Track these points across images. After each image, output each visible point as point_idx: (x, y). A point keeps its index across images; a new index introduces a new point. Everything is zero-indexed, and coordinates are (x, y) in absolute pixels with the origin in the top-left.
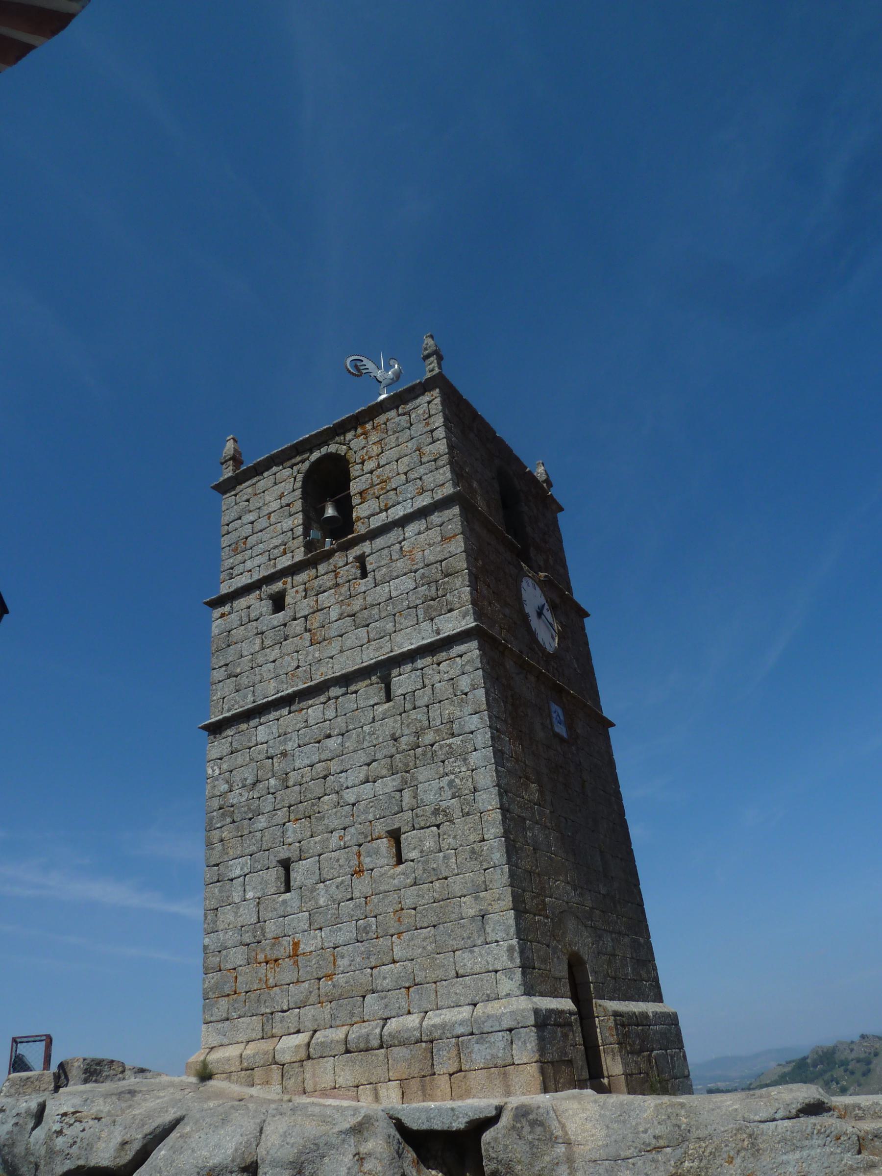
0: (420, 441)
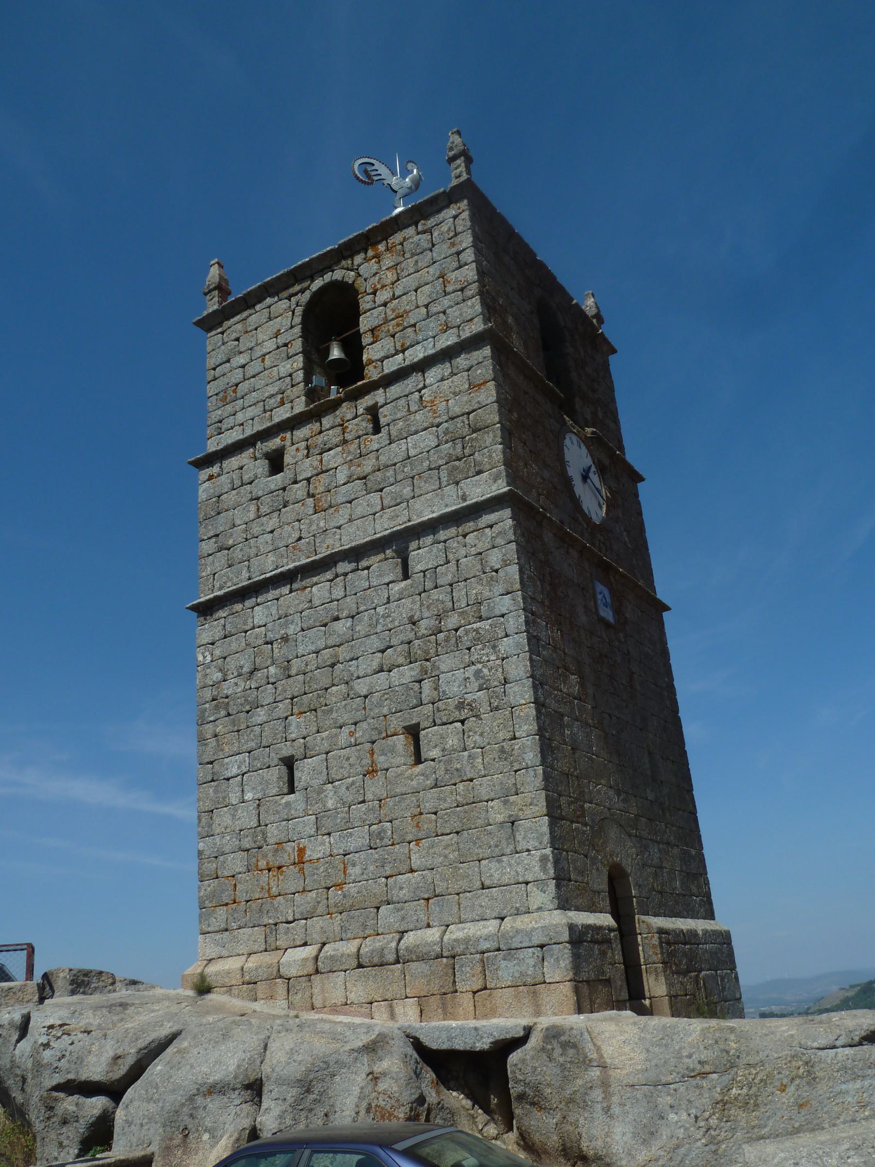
0: (444, 266)
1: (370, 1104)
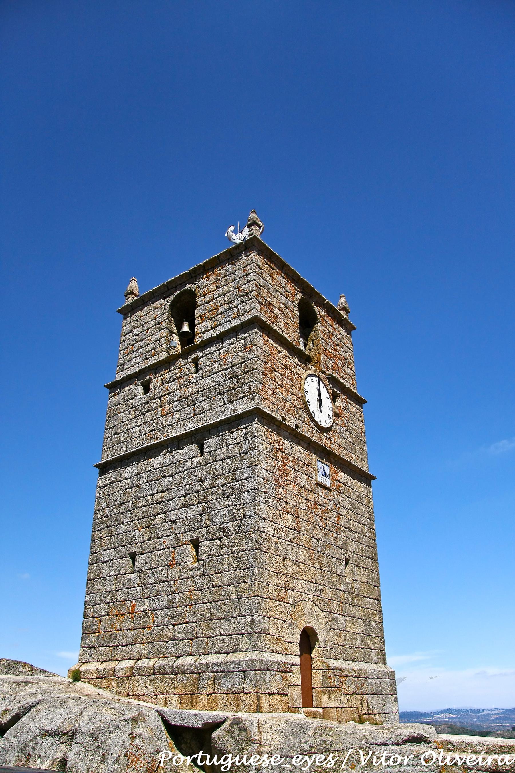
0: (239, 282)
1: (127, 752)
